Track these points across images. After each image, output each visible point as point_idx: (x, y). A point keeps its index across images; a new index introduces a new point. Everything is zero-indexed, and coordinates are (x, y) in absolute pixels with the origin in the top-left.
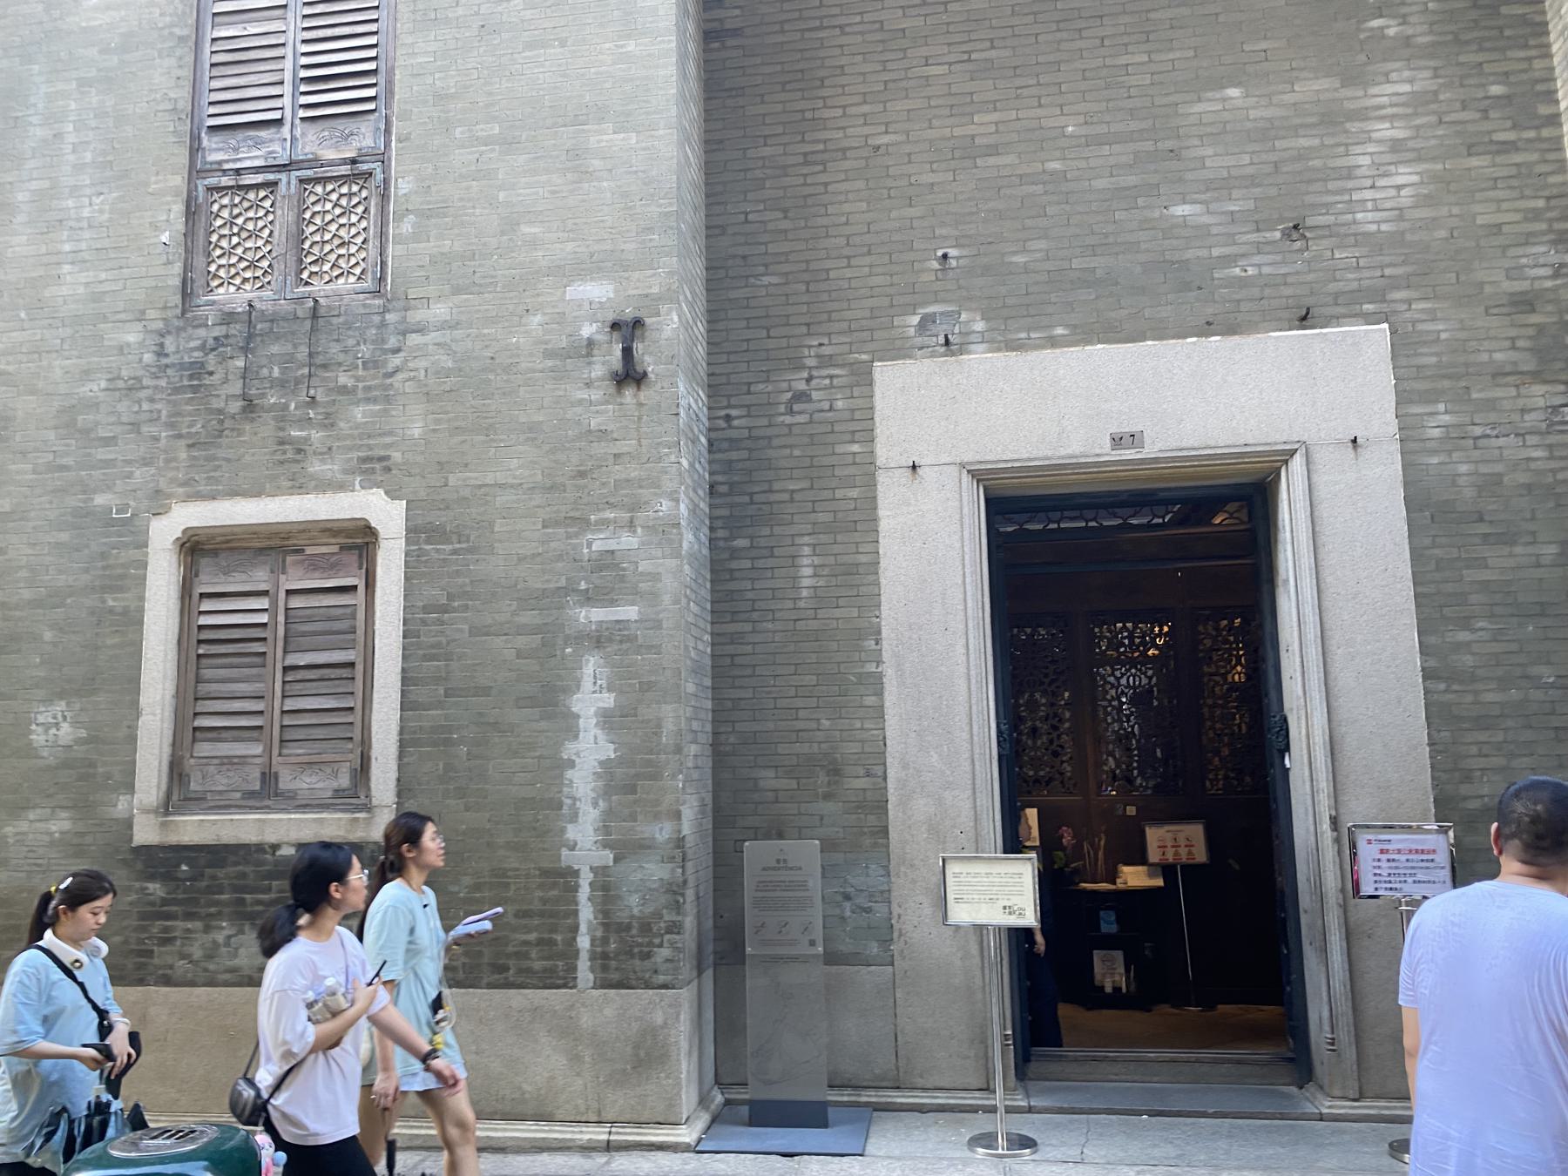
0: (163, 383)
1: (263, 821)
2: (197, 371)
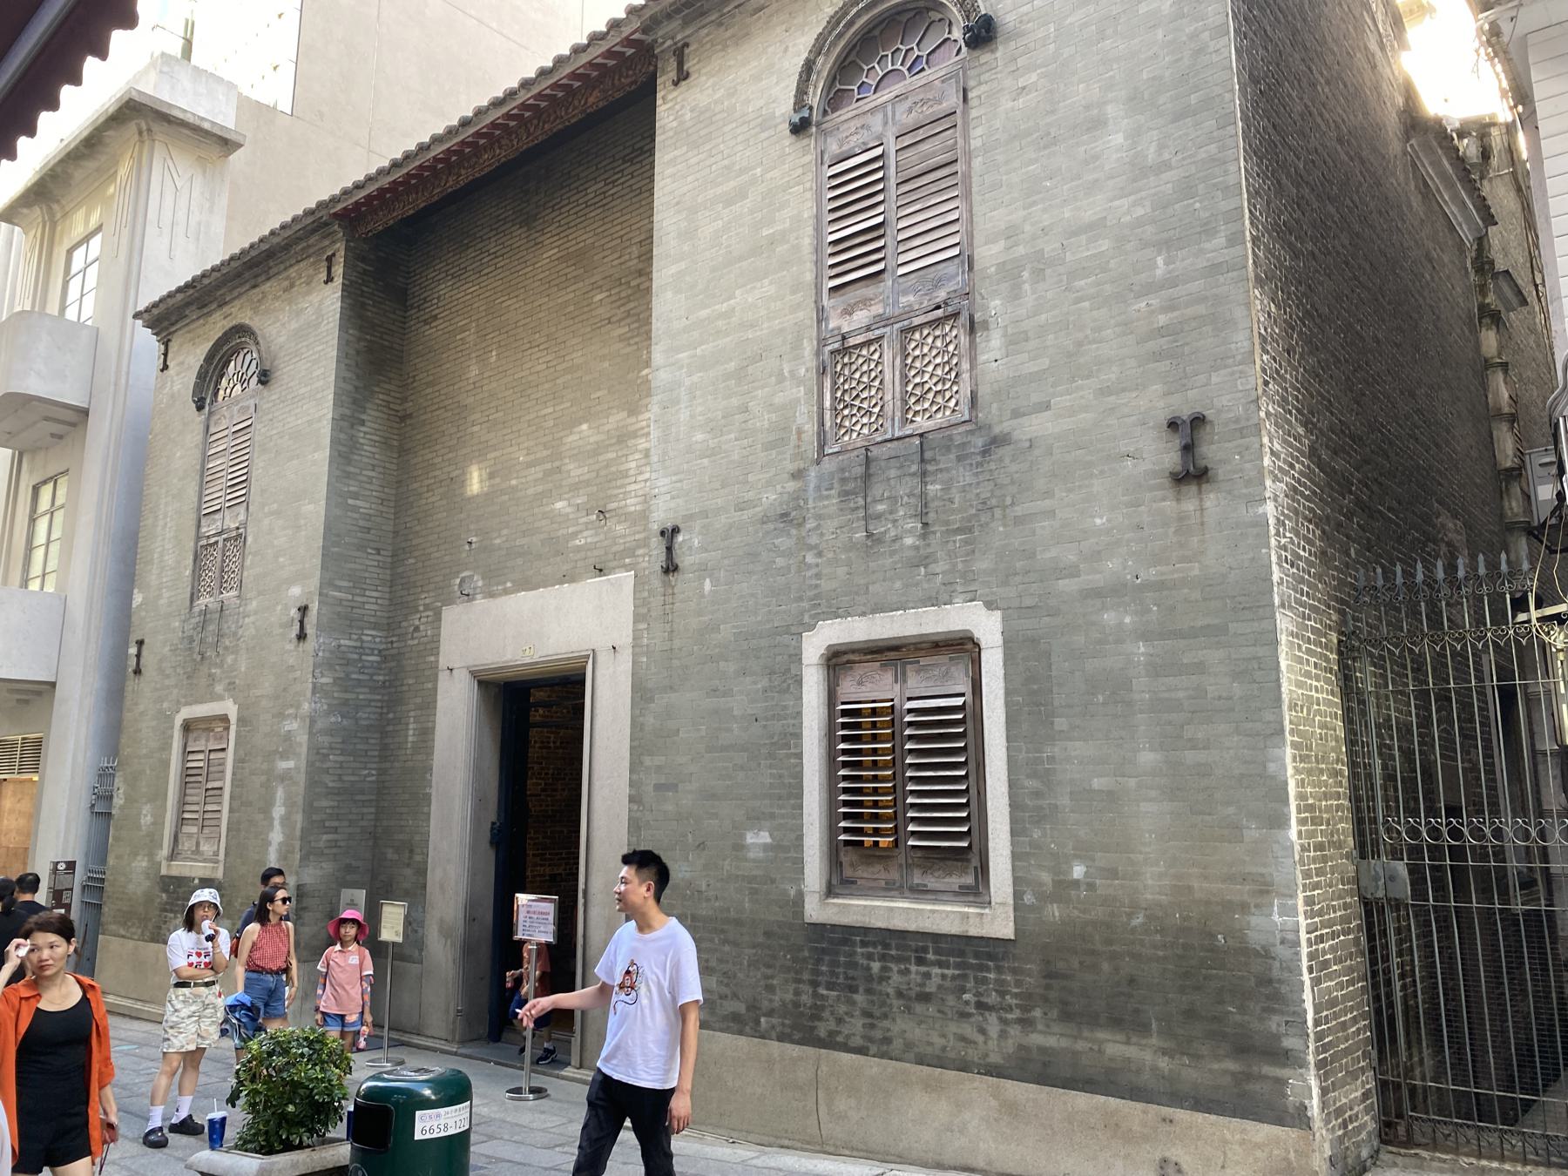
1: (891, 909)
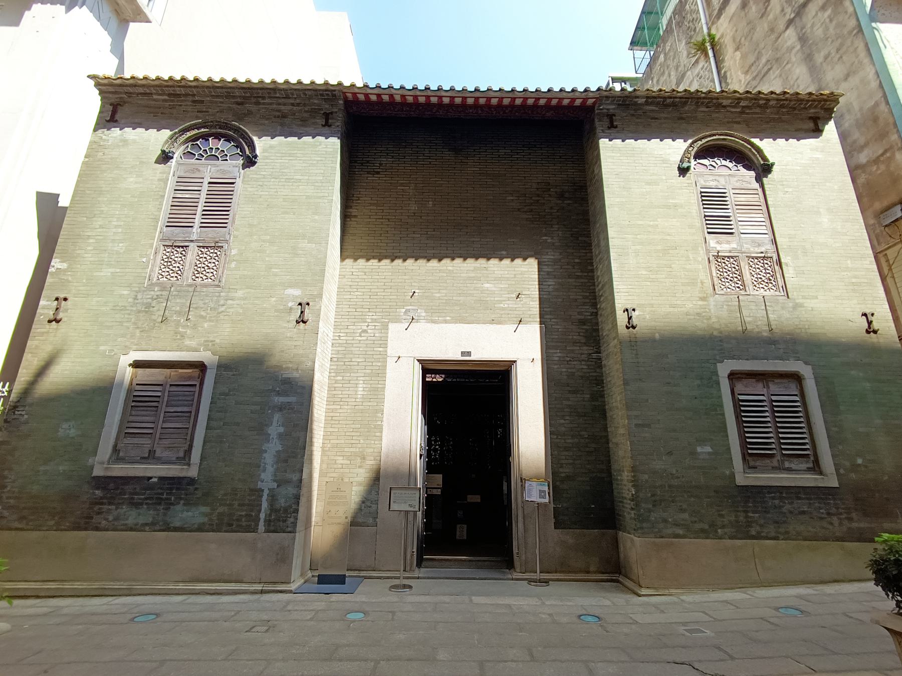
0: (134, 309)
2: (149, 306)
